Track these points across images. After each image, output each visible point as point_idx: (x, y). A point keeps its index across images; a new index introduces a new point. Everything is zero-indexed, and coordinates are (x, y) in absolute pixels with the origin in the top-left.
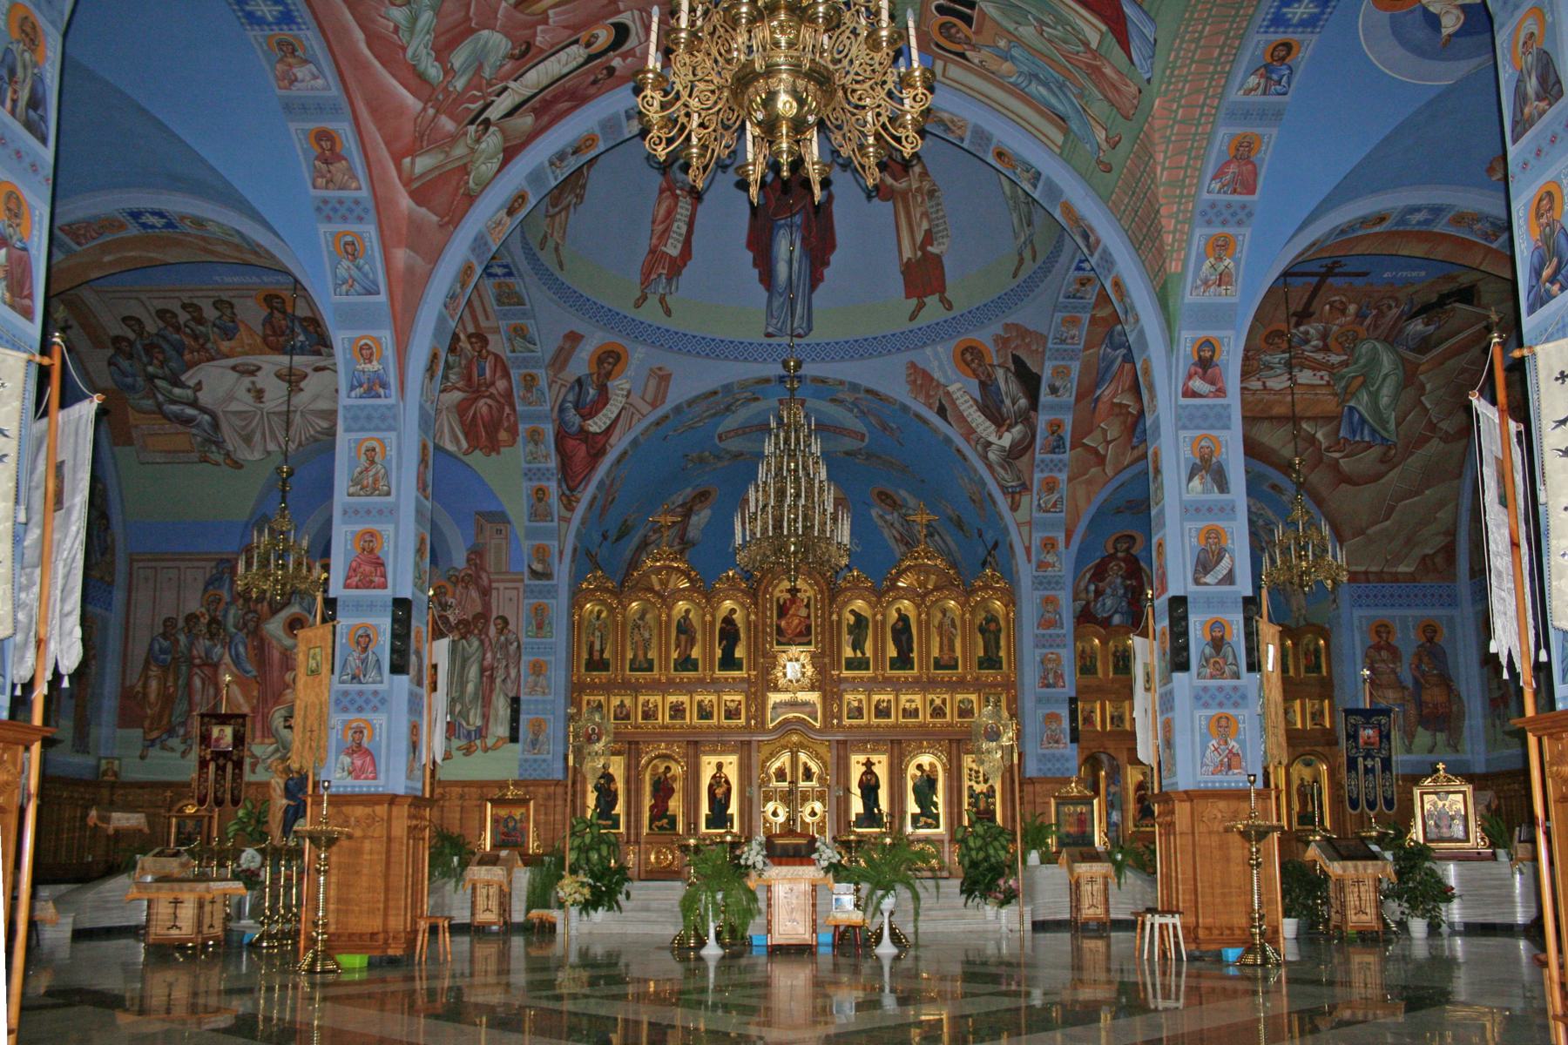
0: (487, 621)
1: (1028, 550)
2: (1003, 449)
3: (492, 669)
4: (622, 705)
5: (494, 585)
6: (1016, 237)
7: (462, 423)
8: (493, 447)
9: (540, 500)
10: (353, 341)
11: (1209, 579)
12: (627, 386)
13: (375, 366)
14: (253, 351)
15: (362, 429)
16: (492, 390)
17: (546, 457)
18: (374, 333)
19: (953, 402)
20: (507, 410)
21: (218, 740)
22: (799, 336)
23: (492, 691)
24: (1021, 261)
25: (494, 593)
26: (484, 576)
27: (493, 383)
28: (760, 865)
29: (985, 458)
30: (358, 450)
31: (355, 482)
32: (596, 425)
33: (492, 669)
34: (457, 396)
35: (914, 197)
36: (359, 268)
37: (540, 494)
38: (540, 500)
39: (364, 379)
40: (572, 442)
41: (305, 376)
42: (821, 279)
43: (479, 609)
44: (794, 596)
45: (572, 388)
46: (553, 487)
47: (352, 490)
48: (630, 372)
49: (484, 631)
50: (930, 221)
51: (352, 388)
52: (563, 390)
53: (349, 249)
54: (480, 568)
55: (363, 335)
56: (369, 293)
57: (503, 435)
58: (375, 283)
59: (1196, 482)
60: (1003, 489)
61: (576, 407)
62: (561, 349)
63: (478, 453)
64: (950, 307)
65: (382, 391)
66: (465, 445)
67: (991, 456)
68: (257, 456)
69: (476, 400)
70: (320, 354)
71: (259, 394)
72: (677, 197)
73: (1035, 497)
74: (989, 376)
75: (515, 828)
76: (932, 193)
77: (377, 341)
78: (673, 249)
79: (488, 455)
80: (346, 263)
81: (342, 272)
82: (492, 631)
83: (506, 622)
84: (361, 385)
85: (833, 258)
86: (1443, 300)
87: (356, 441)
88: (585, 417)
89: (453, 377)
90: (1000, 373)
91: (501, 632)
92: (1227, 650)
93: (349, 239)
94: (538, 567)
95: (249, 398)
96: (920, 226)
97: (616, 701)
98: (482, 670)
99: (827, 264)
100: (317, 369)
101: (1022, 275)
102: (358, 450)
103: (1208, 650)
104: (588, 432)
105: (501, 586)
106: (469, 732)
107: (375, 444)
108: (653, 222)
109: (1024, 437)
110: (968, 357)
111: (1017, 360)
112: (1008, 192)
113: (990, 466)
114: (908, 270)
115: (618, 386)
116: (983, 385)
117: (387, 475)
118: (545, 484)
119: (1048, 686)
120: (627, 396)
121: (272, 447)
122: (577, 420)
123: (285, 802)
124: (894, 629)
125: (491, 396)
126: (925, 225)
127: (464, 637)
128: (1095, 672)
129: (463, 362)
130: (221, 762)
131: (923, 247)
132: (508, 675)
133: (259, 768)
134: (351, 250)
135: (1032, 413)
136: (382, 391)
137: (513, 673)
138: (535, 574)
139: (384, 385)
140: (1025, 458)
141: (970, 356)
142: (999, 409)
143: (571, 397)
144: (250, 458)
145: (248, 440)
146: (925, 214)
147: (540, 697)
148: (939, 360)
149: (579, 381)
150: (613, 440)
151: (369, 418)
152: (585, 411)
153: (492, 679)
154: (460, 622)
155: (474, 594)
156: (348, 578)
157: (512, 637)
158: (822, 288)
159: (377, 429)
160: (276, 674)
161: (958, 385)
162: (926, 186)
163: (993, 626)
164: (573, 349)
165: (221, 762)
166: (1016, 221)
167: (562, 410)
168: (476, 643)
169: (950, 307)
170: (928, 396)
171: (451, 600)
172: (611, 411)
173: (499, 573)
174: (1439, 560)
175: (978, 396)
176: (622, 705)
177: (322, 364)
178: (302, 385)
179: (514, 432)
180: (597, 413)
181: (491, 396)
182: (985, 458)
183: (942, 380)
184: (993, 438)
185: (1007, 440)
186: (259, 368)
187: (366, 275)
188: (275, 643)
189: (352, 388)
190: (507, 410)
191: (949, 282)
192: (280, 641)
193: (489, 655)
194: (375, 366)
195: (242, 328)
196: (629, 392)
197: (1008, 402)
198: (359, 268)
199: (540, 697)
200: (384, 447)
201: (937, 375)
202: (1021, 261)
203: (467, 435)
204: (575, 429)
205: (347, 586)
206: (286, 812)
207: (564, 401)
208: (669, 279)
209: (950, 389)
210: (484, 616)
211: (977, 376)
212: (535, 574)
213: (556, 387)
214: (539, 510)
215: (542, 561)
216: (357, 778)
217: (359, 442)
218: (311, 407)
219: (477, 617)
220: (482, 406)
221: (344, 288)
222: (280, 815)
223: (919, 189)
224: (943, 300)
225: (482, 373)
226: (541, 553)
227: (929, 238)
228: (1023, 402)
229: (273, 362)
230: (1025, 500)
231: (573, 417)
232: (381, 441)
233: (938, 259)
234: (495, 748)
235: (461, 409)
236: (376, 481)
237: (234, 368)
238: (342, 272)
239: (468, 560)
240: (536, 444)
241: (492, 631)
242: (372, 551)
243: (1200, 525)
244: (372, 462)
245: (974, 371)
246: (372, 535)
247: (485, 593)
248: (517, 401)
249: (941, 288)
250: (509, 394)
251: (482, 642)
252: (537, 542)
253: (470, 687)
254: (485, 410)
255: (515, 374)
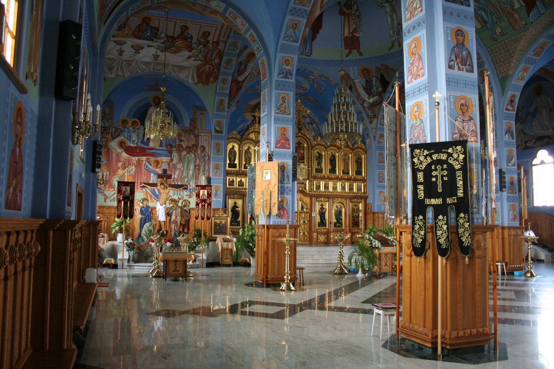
0: (197, 148)
1: (374, 137)
2: (369, 103)
3: (199, 166)
4: (241, 181)
5: (200, 134)
6: (391, 37)
7: (197, 73)
8: (207, 82)
9: (221, 104)
10: (283, 57)
11: (510, 164)
13: (289, 67)
14: (126, 36)
15: (281, 89)
16: (213, 62)
17: (227, 89)
18: (292, 56)
19: (355, 86)
20: (216, 70)
21: (125, 192)
22: (308, 56)
23: (199, 174)
24: (393, 46)
25: (200, 137)
26: (196, 130)
27: (214, 60)
28: (380, 247)
29: (363, 105)
30: (279, 98)
31: (278, 108)
32: (241, 79)
33: (199, 166)
34: (199, 62)
35: (352, 16)
36: (295, 33)
37: (222, 102)
38: (221, 104)
39: (284, 71)
41: (143, 48)
42: (316, 38)
43: (194, 143)
44: (299, 145)
46: (226, 99)
47: (277, 111)
49: (196, 151)
50: (356, 25)
51: (280, 74)
53: (294, 26)
54: (195, 127)
55: (287, 56)
56: (295, 42)
57: (211, 79)
58: (298, 39)
59: (507, 136)
60: (368, 116)
63: (200, 84)
64: (361, 55)
65: (290, 77)
66: (196, 81)
67: (365, 105)
68: (113, 76)
69: (206, 65)
70: (153, 41)
71: (121, 52)
73: (379, 120)
74: (370, 79)
75: (222, 227)
76: (359, 17)
77: (292, 58)
79: (208, 85)
80: (291, 30)
81: (288, 33)
82: (199, 151)
83: (204, 148)
84: (283, 74)
85: (321, 31)
87: (279, 93)
89: (200, 56)
90: (374, 79)
91: (202, 152)
92: (514, 185)
93: (296, 22)
94: (218, 129)
95: (116, 53)
96: (352, 26)
97: (238, 179)
98: (195, 166)
99: (318, 33)
100: (148, 46)
101: (392, 51)
102: (279, 98)
103: (510, 185)
105: (203, 134)
106: (190, 189)
107: (285, 95)
109: (377, 101)
110: (365, 72)
111: (382, 76)
112: (390, 22)
113: (364, 108)
114: (346, 40)
116: (367, 81)
117: (289, 107)
118: (224, 98)
119: (380, 182)
121: (120, 73)
123: (140, 216)
124: (330, 159)
125: (212, 65)
126: (354, 26)
127: (188, 153)
128: (348, 173)
129: (206, 51)
130: (126, 201)
131: (352, 33)
132: (205, 168)
133: (108, 200)
134: (295, 26)
135: (383, 93)
136: (290, 77)
137: (207, 168)
138: (216, 131)
139: (291, 75)
140: (377, 107)
141: (365, 72)
142: (370, 90)
144: (110, 76)
145: (111, 69)
146: (354, 23)
147: (218, 177)
148: (354, 72)
150: (244, 84)
151: (284, 86)
153: (199, 169)
154: (187, 147)
155: (192, 137)
156: (277, 144)
157: (206, 154)
158: (316, 40)
159: (286, 90)
160: (114, 163)
161: (358, 80)
162: (357, 14)
163: (360, 161)
165: (126, 201)
166: (391, 32)
168: (193, 156)
169: (361, 55)
170: (347, 82)
171: (183, 139)
172: (246, 74)
173: (202, 129)
175: (364, 84)
176: (241, 181)
177: (152, 45)
178: (140, 51)
179: (216, 78)
181: (212, 65)
182: (363, 105)
183: (353, 78)
184: (366, 99)
185: (371, 100)
186: (126, 43)
187: (296, 36)
188: (113, 150)
189: (280, 74)
190: (216, 70)
191: (361, 47)
192: (115, 150)
193: (198, 160)
194: (289, 67)
195: (127, 27)
197: (374, 88)
198: (295, 33)
199: (218, 177)
200: (288, 97)
201: (352, 76)
202: (393, 46)
203: (198, 77)
205: (276, 147)
206: (141, 220)
209: (355, 81)
210: (196, 146)
211: (366, 78)
212: (216, 131)
214: (220, 108)
215: (220, 127)
216: (282, 218)
217: (280, 94)
218: (142, 60)
219: (193, 146)
220: (207, 67)
221: (287, 38)
222: (138, 221)
223: (354, 14)
224: (359, 52)
225: (212, 55)
226: (219, 124)
227: (355, 30)
228: (380, 89)
229: (132, 41)
230: (375, 121)
231: (236, 75)
232: (287, 94)
233: (358, 38)
235: (198, 68)
236: (285, 109)
237: (115, 42)
238: (288, 33)
239: (190, 124)
240: (224, 83)
241: (199, 151)
242: (285, 135)
243: (508, 148)
244: (284, 102)
245: (365, 77)
246: (285, 129)
247: (197, 137)
248: (222, 67)
249: (358, 48)
250: (219, 64)
251: (195, 155)
252: (218, 120)
253: (191, 172)
254: (208, 69)
255: (225, 58)
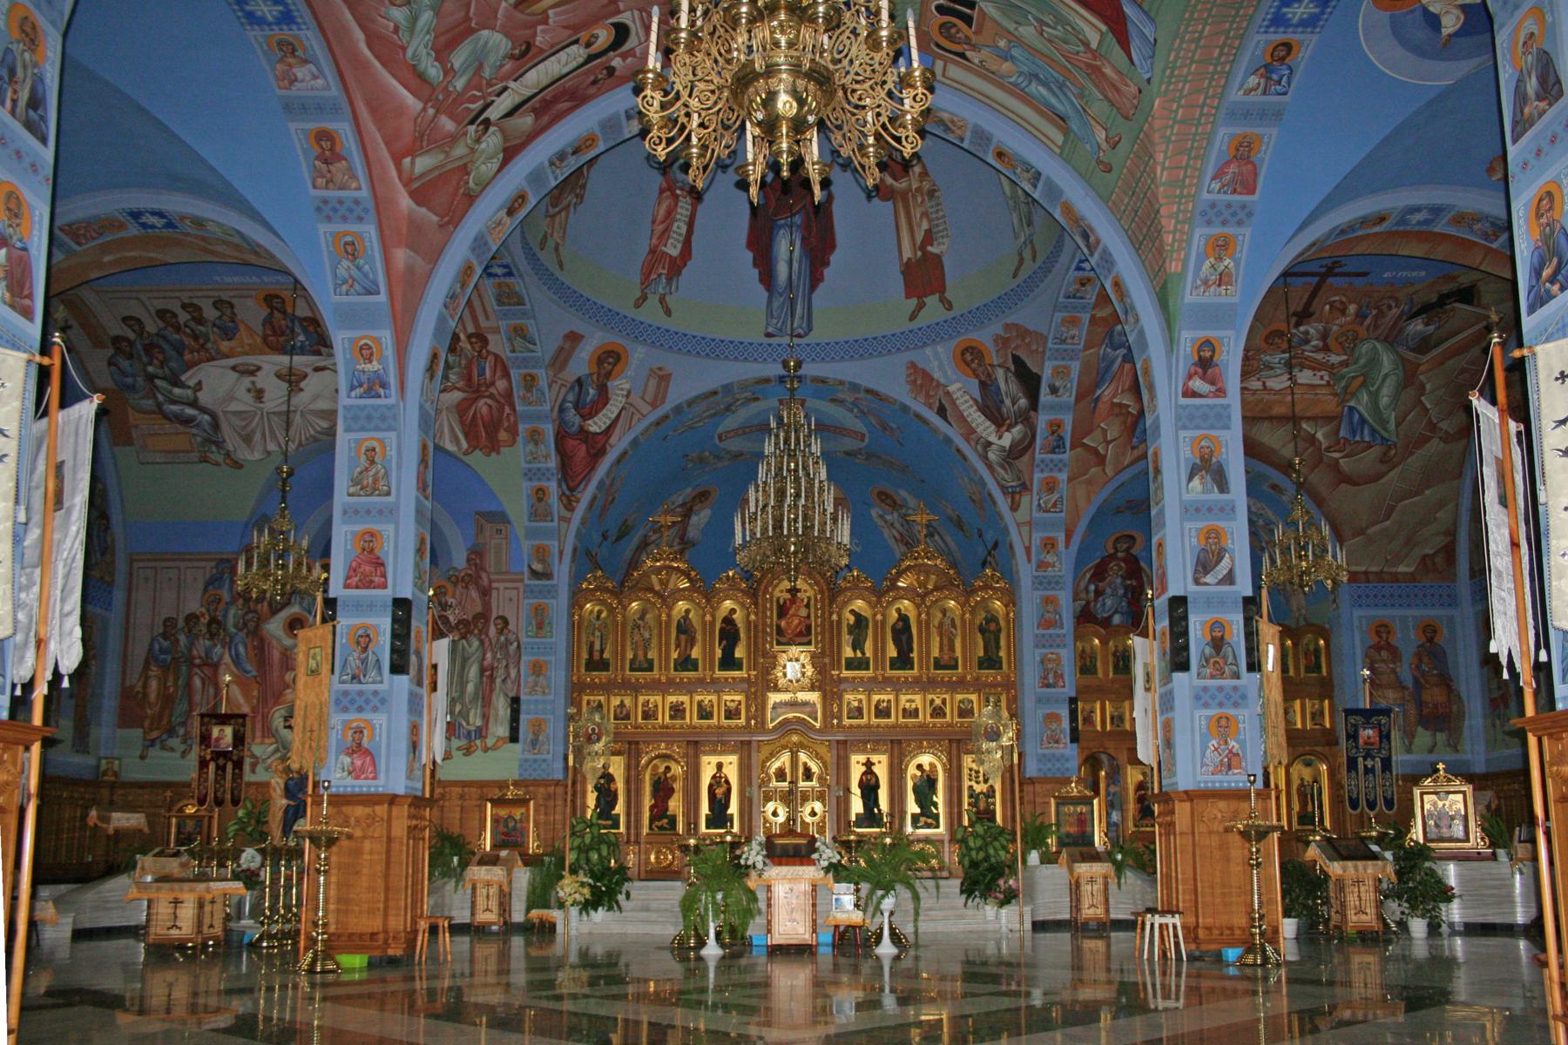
0: (487, 621)
1: (1028, 550)
2: (1003, 449)
3: (492, 669)
4: (622, 705)
5: (494, 585)
6: (1016, 237)
7: (462, 423)
8: (493, 447)
9: (540, 500)
10: (353, 341)
11: (1209, 579)
12: (627, 386)
13: (375, 366)
14: (253, 351)
15: (362, 429)
16: (492, 390)
17: (546, 457)
18: (374, 333)
19: (953, 402)
20: (507, 410)
21: (218, 740)
22: (799, 336)
23: (492, 691)
24: (1021, 261)
25: (494, 593)
26: (484, 576)
27: (493, 383)
29: (985, 458)
30: (358, 450)
31: (355, 482)
32: (596, 425)
33: (492, 669)
34: (457, 396)
35: (914, 197)
36: (359, 268)
37: (540, 494)
38: (540, 500)
39: (364, 379)
40: (572, 442)
41: (305, 376)
42: (821, 279)
43: (479, 609)
44: (794, 596)
45: (572, 388)
46: (553, 487)
47: (352, 490)
48: (630, 372)
49: (484, 631)
50: (930, 221)
51: (352, 388)
52: (563, 390)
53: (349, 249)
54: (480, 568)
55: (363, 335)
56: (369, 293)
57: (503, 435)
58: (375, 283)
60: (1003, 489)
61: (576, 407)
62: (561, 349)
63: (478, 453)
64: (950, 307)
65: (382, 391)
66: (465, 445)
67: (991, 456)
68: (257, 456)
69: (476, 400)
70: (320, 354)
71: (259, 394)
72: (677, 197)
73: (1035, 497)
74: (989, 376)
75: (515, 828)
76: (932, 193)
77: (377, 341)
78: (673, 249)
79: (488, 455)
80: (346, 263)
81: (342, 272)
82: (492, 631)
83: (506, 622)
84: (361, 385)
85: (833, 258)
86: (1443, 300)
87: (356, 441)
88: (585, 417)
89: (453, 377)
90: (1000, 373)
91: (501, 632)
92: (1227, 650)
93: (349, 239)
94: (538, 567)
95: (249, 398)
96: (920, 226)
97: (616, 701)
98: (482, 670)
99: (827, 264)
100: (317, 369)
101: (1022, 275)
102: (358, 450)
103: (1208, 650)
104: (588, 432)
105: (501, 586)
106: (469, 732)
107: (375, 444)
108: (653, 222)
109: (1024, 437)
110: (968, 357)
111: (1017, 360)
112: (1008, 192)
113: (990, 466)
114: (908, 270)
115: (618, 386)
116: (983, 385)
117: (387, 475)
118: (545, 484)
119: (1048, 686)
120: (627, 396)
121: (272, 447)
122: (577, 420)
123: (285, 802)
124: (894, 629)
125: (491, 396)
126: (925, 225)
127: (464, 637)
128: (1095, 672)
129: (463, 362)
130: (221, 762)
131: (923, 247)
132: (508, 675)
133: (259, 768)
134: (351, 250)
135: (1032, 413)
136: (382, 391)
137: (513, 673)
138: (535, 574)
139: (384, 385)
140: (1025, 458)
141: (970, 356)
142: (999, 409)
143: (571, 397)
144: (250, 458)
145: (248, 440)
146: (925, 214)
147: (540, 697)
148: (939, 360)
149: (579, 381)
150: (613, 440)
151: (369, 418)
152: (585, 411)
153: (492, 679)
154: (460, 622)
155: (474, 594)
156: (348, 578)
157: (512, 637)
158: (822, 288)
159: (377, 429)
160: (276, 674)
161: (958, 385)
162: (926, 186)
163: (993, 626)
164: (573, 349)
165: (221, 762)
166: (1016, 221)
167: (562, 410)
168: (476, 643)
169: (950, 307)
170: (928, 396)
171: (451, 600)
172: (611, 411)
173: (499, 573)
174: (1439, 560)
175: (978, 396)
176: (622, 705)
177: (322, 364)
178: (302, 385)
179: (514, 432)
180: (597, 413)
181: (491, 396)
182: (985, 458)
183: (942, 380)
184: (993, 438)
185: (1007, 440)
186: (259, 368)
187: (366, 275)
188: (275, 643)
189: (352, 388)
190: (507, 410)
191: (949, 282)
192: (280, 641)
193: (489, 655)
194: (375, 366)
195: (242, 328)
196: (629, 392)
197: (1008, 402)
198: (359, 268)
199: (540, 697)
200: (384, 447)
201: (937, 375)
202: (1021, 261)
203: (467, 435)
204: (575, 429)
205: (347, 586)
206: (286, 812)
207: (564, 401)
208: (669, 279)
209: (950, 389)
210: (484, 616)
211: (977, 376)
212: (535, 574)
213: (556, 387)
214: (539, 510)
215: (542, 561)
217: (359, 442)
218: (311, 407)
219: (477, 617)
220: (482, 406)
221: (344, 288)
222: (280, 815)
223: (919, 189)
224: (943, 300)
225: (482, 373)
226: (541, 553)
227: (929, 238)
228: (1023, 402)
229: (273, 362)
230: (1025, 500)
231: (573, 417)
232: (381, 441)
233: (938, 259)
234: (495, 748)
235: (461, 409)
236: (376, 481)
237: (234, 368)
238: (342, 272)
239: (468, 560)
240: (536, 444)
241: (492, 631)
242: (372, 551)
243: (1200, 525)
244: (372, 462)
245: (974, 371)
246: (372, 535)
247: (485, 593)
248: (517, 401)
249: (941, 288)
250: (509, 394)
251: (482, 642)
252: (537, 542)
253: (470, 687)
254: (485, 410)
255: (515, 374)
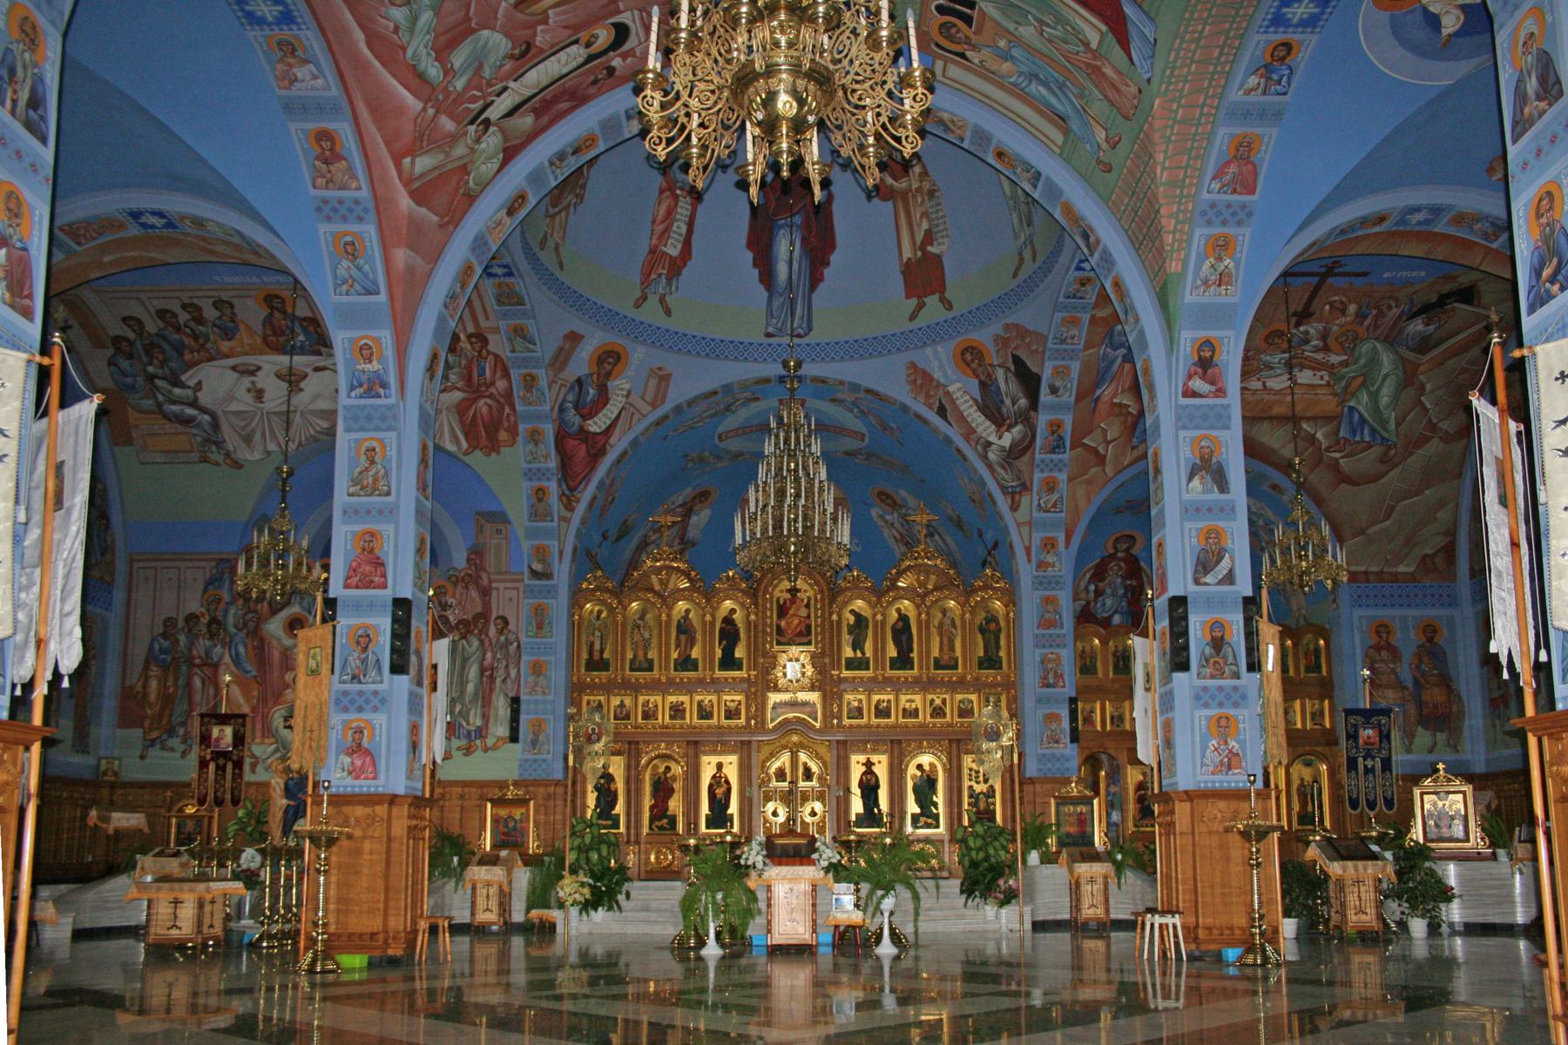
0: (487, 621)
1: (1028, 550)
2: (1003, 449)
3: (492, 669)
4: (622, 705)
5: (494, 585)
6: (1016, 237)
7: (462, 423)
8: (493, 447)
9: (540, 500)
10: (353, 341)
11: (1209, 579)
12: (627, 386)
13: (375, 366)
14: (253, 351)
15: (362, 429)
16: (492, 390)
17: (546, 457)
18: (374, 333)
19: (953, 402)
20: (507, 410)
21: (218, 740)
22: (799, 336)
23: (492, 691)
24: (1021, 261)
25: (494, 593)
26: (484, 576)
27: (493, 383)
28: (760, 865)
29: (985, 458)
30: (358, 450)
31: (355, 482)
32: (596, 425)
33: (492, 669)
34: (457, 396)
35: (914, 197)
36: (359, 268)
37: (540, 494)
38: (540, 500)
39: (364, 379)
40: (572, 442)
41: (305, 376)
42: (821, 279)
43: (479, 609)
44: (794, 596)
45: (572, 388)
46: (553, 487)
47: (352, 490)
48: (630, 372)
49: (484, 631)
50: (930, 221)
51: (352, 388)
52: (563, 390)
53: (349, 249)
54: (480, 568)
55: (363, 335)
56: (369, 293)
57: (503, 435)
58: (375, 283)
60: (1003, 489)
61: (576, 407)
62: (561, 349)
63: (478, 453)
64: (950, 307)
65: (382, 391)
66: (465, 445)
67: (991, 456)
68: (257, 456)
69: (476, 400)
70: (320, 354)
71: (259, 394)
72: (677, 197)
73: (1035, 497)
74: (989, 376)
75: (515, 828)
76: (932, 193)
77: (377, 341)
78: (673, 249)
79: (488, 455)
80: (346, 263)
81: (342, 272)
82: (492, 631)
83: (506, 622)
84: (361, 385)
85: (833, 258)
87: (356, 441)
88: (585, 417)
89: (453, 377)
90: (1000, 373)
91: (501, 632)
92: (1227, 650)
93: (349, 239)
94: (538, 567)
95: (249, 398)
96: (920, 226)
97: (616, 701)
98: (482, 670)
99: (827, 264)
100: (317, 369)
101: (1022, 275)
102: (358, 450)
103: (1208, 650)
104: (588, 432)
105: (501, 586)
106: (469, 732)
107: (375, 444)
108: (653, 222)
109: (1024, 437)
110: (968, 357)
111: (1017, 360)
112: (1008, 192)
113: (990, 466)
114: (908, 270)
115: (618, 386)
116: (983, 385)
117: (387, 475)
118: (545, 484)
119: (1048, 686)
120: (627, 396)
121: (272, 447)
122: (577, 420)
123: (285, 802)
124: (894, 629)
125: (491, 396)
126: (925, 225)
127: (464, 637)
128: (1095, 672)
129: (463, 362)
130: (221, 762)
131: (923, 247)
132: (508, 675)
133: (259, 768)
134: (351, 250)
135: (1032, 413)
136: (382, 391)
137: (513, 673)
138: (535, 574)
139: (384, 385)
140: (1025, 458)
141: (970, 356)
142: (999, 409)
143: (571, 397)
144: (250, 458)
145: (248, 440)
146: (925, 214)
147: (540, 697)
148: (939, 360)
149: (579, 381)
150: (613, 440)
151: (369, 418)
152: (585, 411)
153: (492, 679)
154: (460, 622)
155: (474, 594)
156: (348, 578)
157: (512, 637)
158: (822, 288)
159: (377, 429)
160: (276, 674)
161: (958, 385)
162: (926, 186)
163: (993, 626)
164: (573, 349)
165: (221, 762)
166: (1016, 221)
167: (562, 410)
168: (476, 643)
169: (950, 307)
170: (928, 396)
171: (451, 600)
172: (611, 411)
173: (499, 573)
174: (1439, 560)
175: (978, 396)
176: (622, 705)
177: (322, 364)
178: (302, 385)
179: (514, 432)
180: (597, 413)
181: (491, 396)
182: (985, 458)
183: (942, 380)
184: (993, 438)
185: (1007, 440)
186: (259, 368)
187: (366, 275)
188: (275, 643)
189: (352, 388)
190: (507, 410)
191: (949, 282)
192: (280, 641)
193: (489, 655)
194: (375, 366)
195: (242, 328)
196: (629, 392)
197: (1008, 402)
198: (359, 268)
199: (540, 697)
200: (384, 447)
201: (937, 375)
202: (1021, 261)
203: (467, 435)
204: (575, 429)
205: (347, 586)
206: (286, 812)
207: (564, 401)
208: (669, 279)
209: (950, 389)
210: (484, 616)
211: (977, 376)
212: (535, 574)
213: (556, 387)
214: (539, 510)
215: (542, 561)
216: (357, 778)
217: (359, 442)
218: (311, 407)
219: (477, 617)
220: (482, 406)
221: (344, 288)
222: (280, 815)
223: (919, 189)
224: (943, 300)
225: (482, 373)
226: (541, 553)
227: (929, 238)
228: (1023, 402)
229: (273, 362)
230: (1025, 500)
231: (573, 417)
232: (381, 441)
233: (938, 259)
235: (461, 409)
236: (376, 481)
237: (234, 368)
238: (342, 272)
239: (468, 560)
240: (536, 444)
241: (492, 631)
242: (372, 551)
244: (372, 462)
245: (974, 371)
246: (372, 535)
247: (485, 593)
248: (517, 401)
249: (941, 288)
250: (509, 394)
251: (482, 642)
252: (537, 542)
253: (470, 687)
254: (485, 410)
255: (515, 374)
